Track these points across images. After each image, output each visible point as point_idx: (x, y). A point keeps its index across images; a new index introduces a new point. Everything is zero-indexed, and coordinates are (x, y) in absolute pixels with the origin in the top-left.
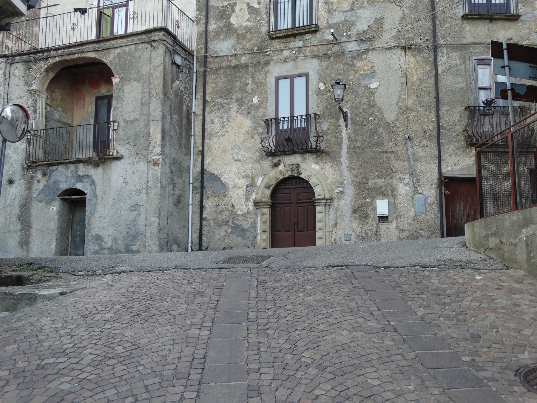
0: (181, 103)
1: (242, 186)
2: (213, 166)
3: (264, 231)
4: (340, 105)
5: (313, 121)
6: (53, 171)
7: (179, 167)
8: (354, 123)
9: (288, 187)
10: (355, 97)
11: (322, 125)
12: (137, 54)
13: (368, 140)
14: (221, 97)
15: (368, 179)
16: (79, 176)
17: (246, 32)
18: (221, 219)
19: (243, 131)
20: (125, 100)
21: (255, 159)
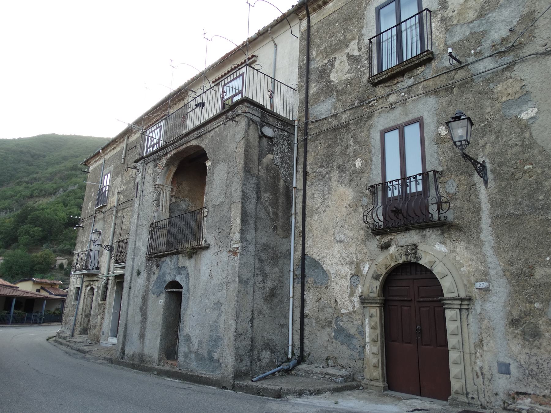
0: (276, 178)
1: (346, 275)
2: (314, 250)
3: (374, 341)
4: (464, 151)
5: (432, 181)
6: (163, 262)
7: (274, 254)
8: (499, 176)
9: (405, 277)
10: (497, 137)
11: (447, 186)
12: (225, 133)
13: (526, 202)
14: (321, 166)
15: (532, 268)
16: (179, 267)
17: (346, 86)
18: (324, 318)
19: (345, 203)
20: (214, 183)
21: (360, 239)
